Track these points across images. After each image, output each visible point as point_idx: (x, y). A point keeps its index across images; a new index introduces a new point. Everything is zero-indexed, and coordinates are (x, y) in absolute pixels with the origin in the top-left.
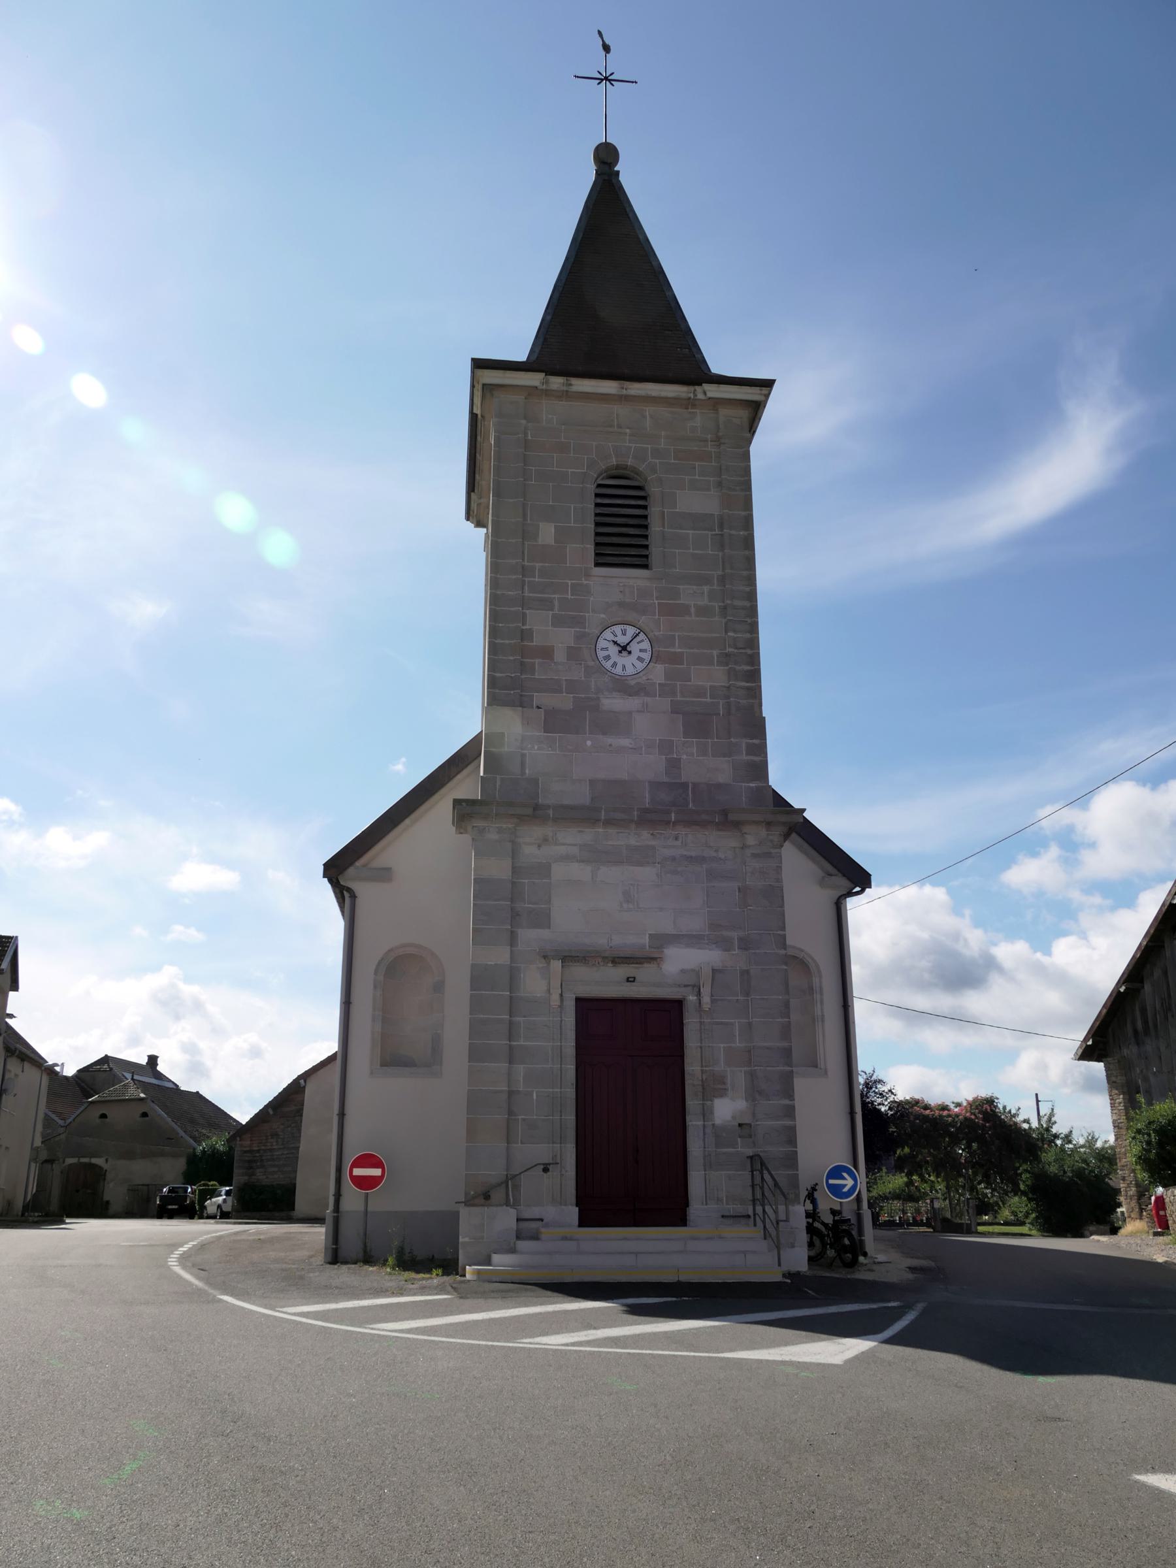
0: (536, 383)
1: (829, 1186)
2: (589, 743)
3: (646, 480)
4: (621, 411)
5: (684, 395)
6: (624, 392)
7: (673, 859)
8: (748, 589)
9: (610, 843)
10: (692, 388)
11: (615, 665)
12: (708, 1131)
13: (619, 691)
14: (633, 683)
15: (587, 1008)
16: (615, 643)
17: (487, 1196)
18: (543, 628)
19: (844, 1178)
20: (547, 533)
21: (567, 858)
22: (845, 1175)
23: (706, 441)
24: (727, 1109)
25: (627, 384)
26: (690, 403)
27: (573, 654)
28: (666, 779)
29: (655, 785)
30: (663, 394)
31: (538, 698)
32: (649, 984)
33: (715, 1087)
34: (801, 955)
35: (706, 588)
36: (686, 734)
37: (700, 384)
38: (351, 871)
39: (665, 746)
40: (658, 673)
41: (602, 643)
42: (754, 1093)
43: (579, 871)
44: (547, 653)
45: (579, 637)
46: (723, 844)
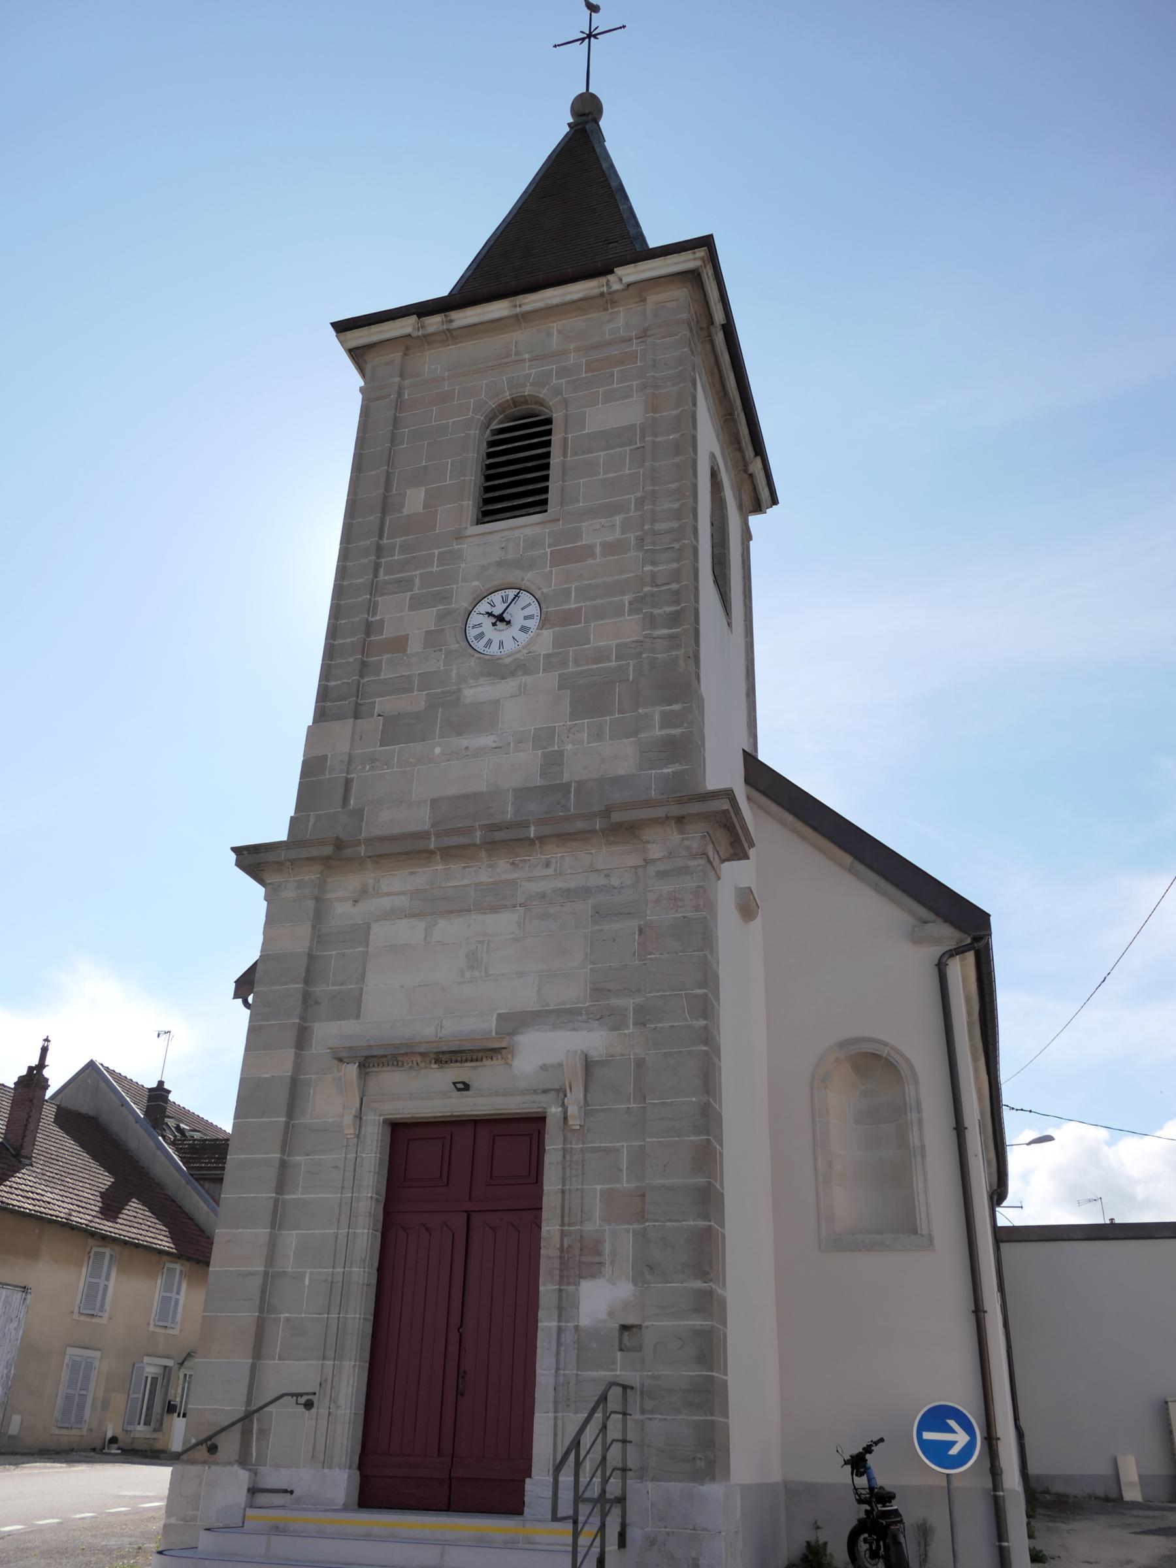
0: (408, 330)
1: (926, 1446)
4: (522, 337)
6: (518, 310)
7: (543, 896)
9: (453, 884)
10: (603, 280)
12: (568, 1337)
13: (489, 675)
15: (403, 1134)
16: (490, 614)
17: (213, 1449)
18: (401, 617)
19: (952, 1431)
20: (414, 500)
21: (391, 914)
22: (952, 1423)
24: (599, 1300)
25: (521, 299)
27: (433, 639)
29: (522, 793)
30: (568, 298)
32: (493, 1093)
33: (583, 1261)
34: (885, 1051)
35: (618, 519)
37: (612, 272)
41: (475, 619)
42: (645, 1270)
43: (407, 931)
44: (399, 645)
46: (610, 863)
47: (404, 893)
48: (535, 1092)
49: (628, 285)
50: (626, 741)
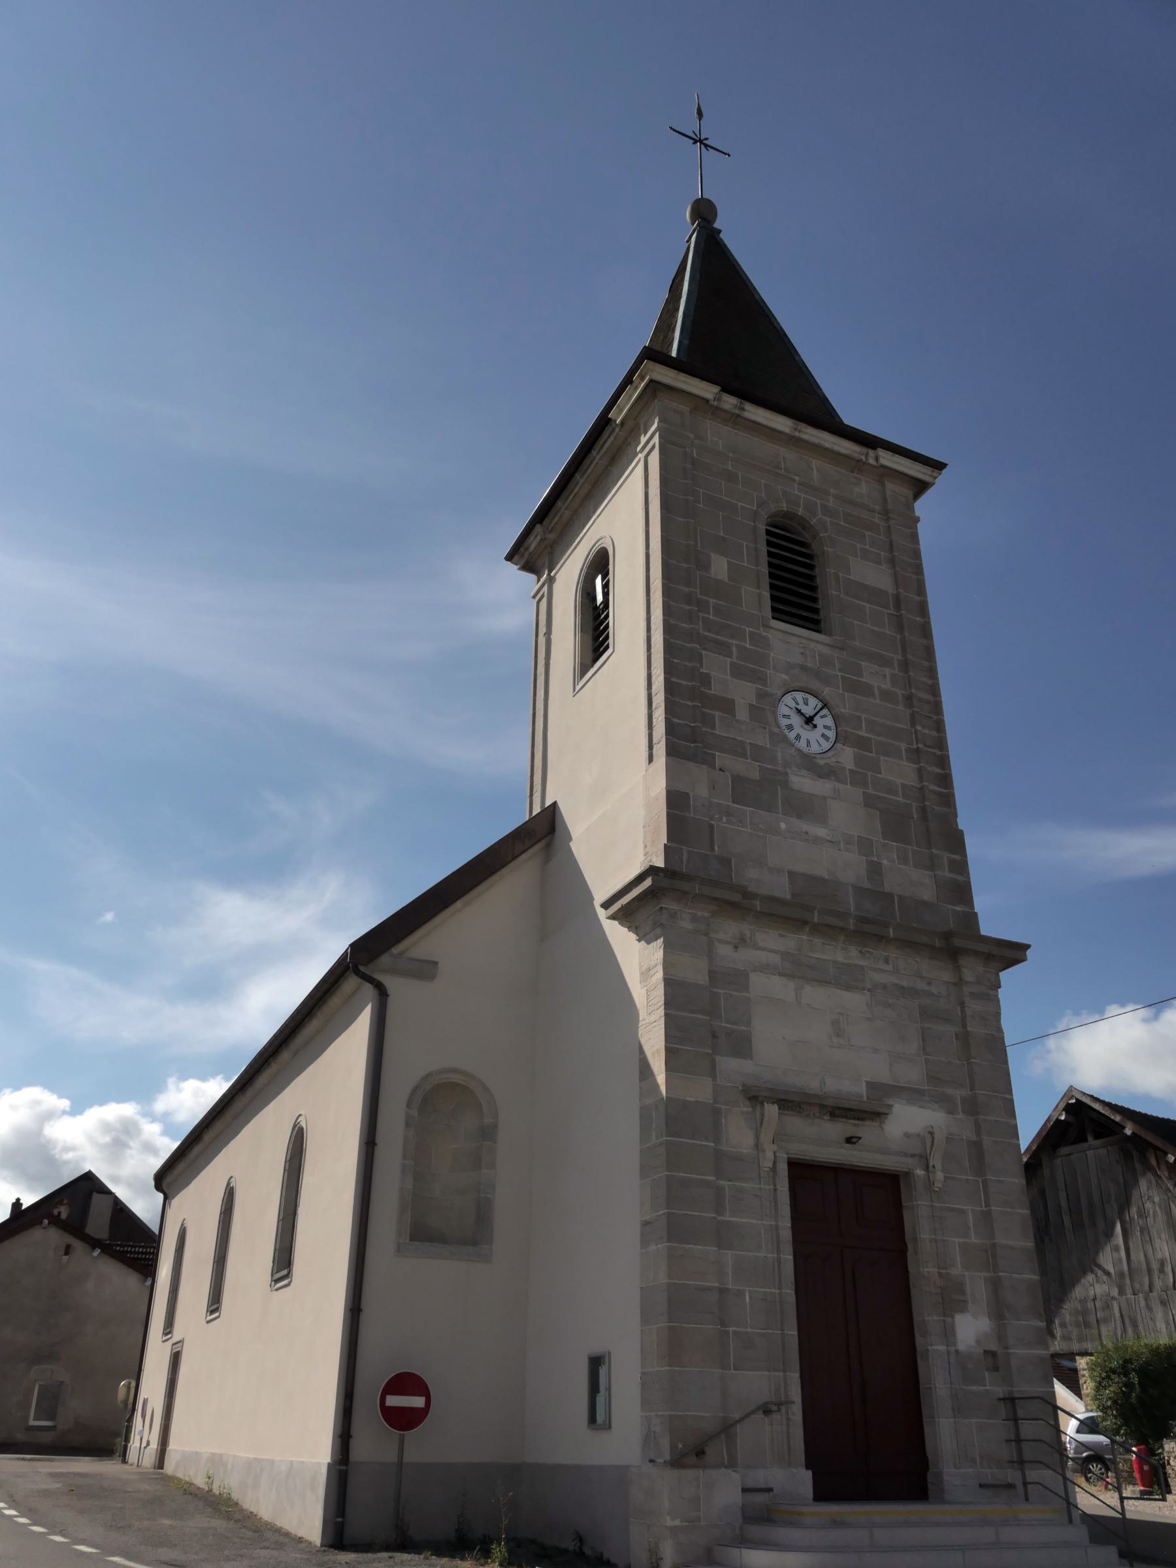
0: (710, 396)
4: (788, 455)
6: (797, 434)
7: (885, 987)
8: (930, 682)
10: (864, 450)
11: (798, 737)
14: (822, 762)
17: (700, 1453)
20: (720, 567)
21: (765, 968)
23: (873, 511)
24: (971, 1329)
26: (858, 466)
28: (867, 885)
29: (860, 891)
30: (836, 448)
31: (721, 759)
33: (952, 1300)
35: (887, 671)
37: (874, 448)
38: (385, 959)
39: (865, 846)
40: (847, 757)
42: (999, 1311)
43: (781, 988)
44: (728, 706)
45: (762, 695)
47: (776, 952)
48: (906, 1155)
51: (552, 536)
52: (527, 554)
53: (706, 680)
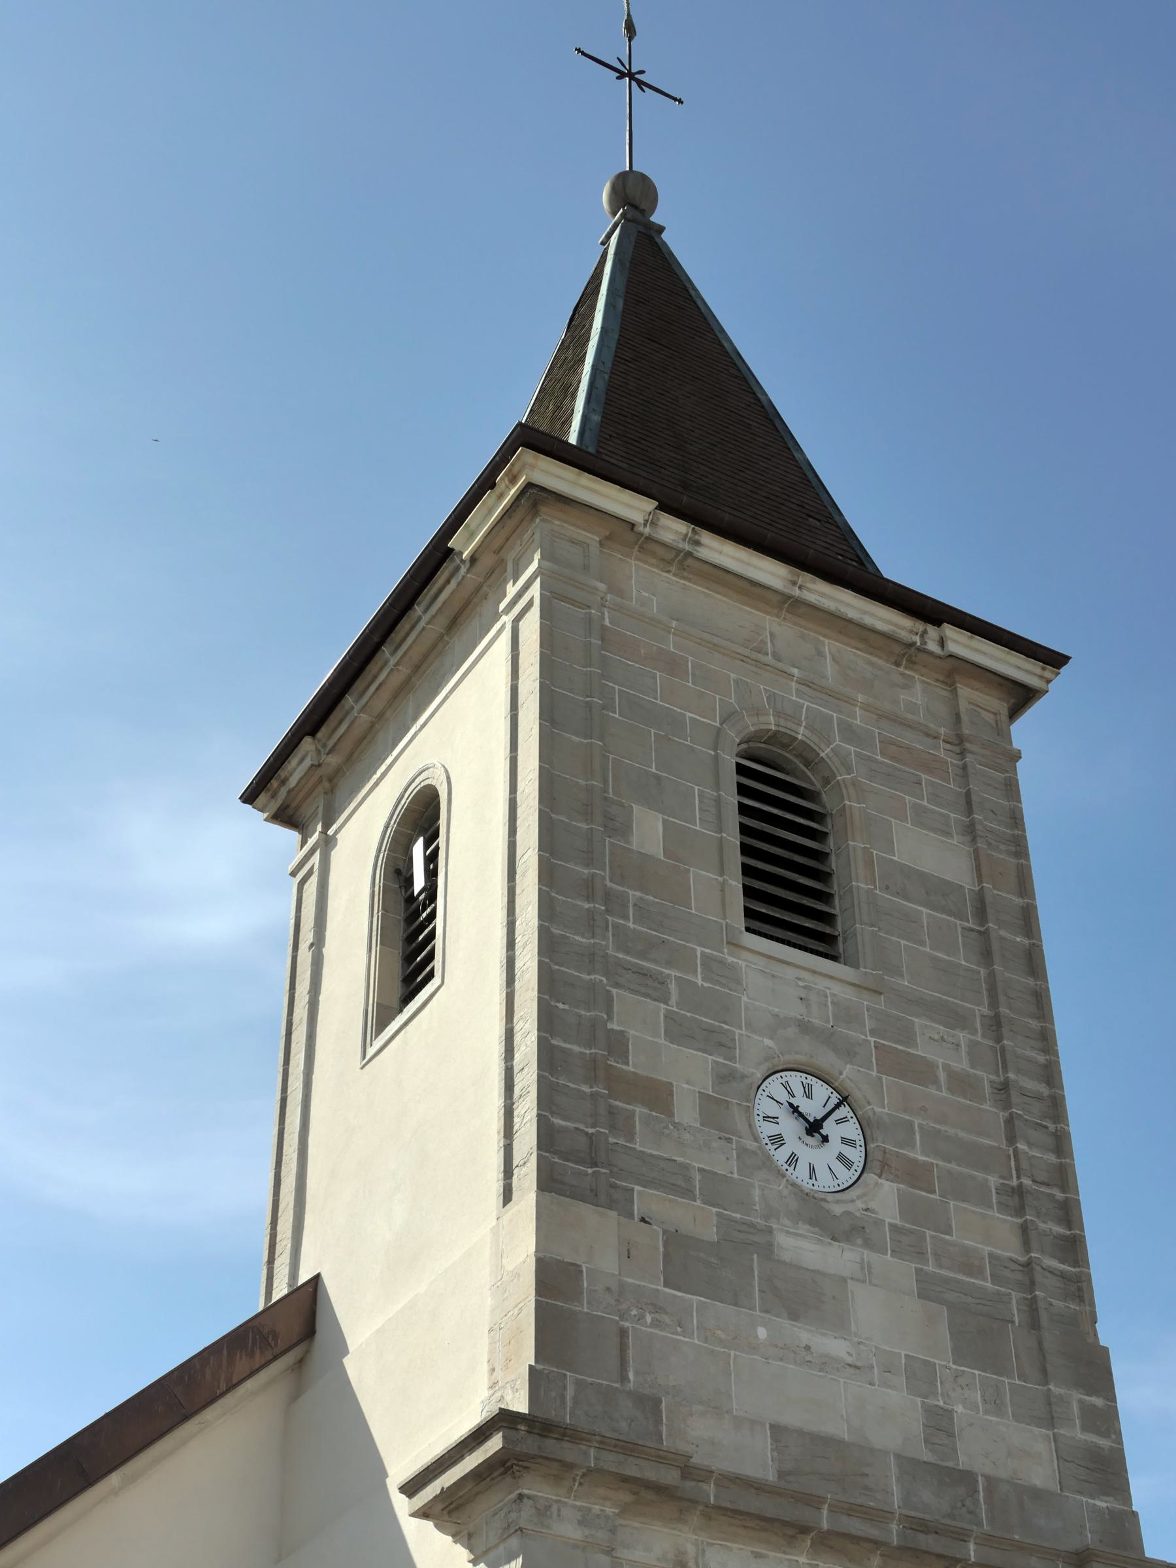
0: (637, 517)
2: (762, 1333)
3: (826, 781)
4: (778, 630)
5: (903, 635)
6: (796, 592)
10: (920, 626)
11: (793, 1160)
20: (649, 831)
25: (806, 578)
28: (926, 1456)
29: (910, 1467)
30: (868, 621)
31: (645, 1199)
35: (962, 1036)
36: (959, 1356)
37: (937, 623)
39: (920, 1377)
40: (885, 1199)
41: (764, 1106)
44: (658, 1096)
45: (725, 1077)
49: (951, 656)
50: (1036, 1430)
51: (333, 760)
52: (283, 792)
53: (618, 1045)
